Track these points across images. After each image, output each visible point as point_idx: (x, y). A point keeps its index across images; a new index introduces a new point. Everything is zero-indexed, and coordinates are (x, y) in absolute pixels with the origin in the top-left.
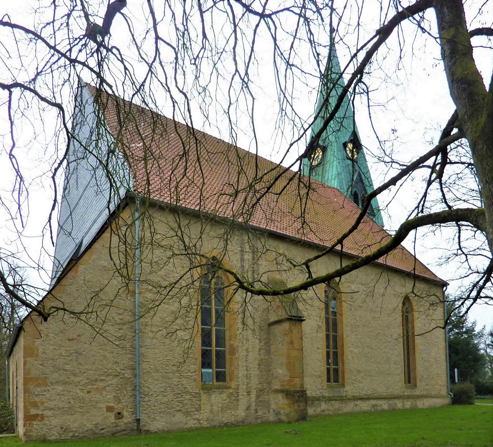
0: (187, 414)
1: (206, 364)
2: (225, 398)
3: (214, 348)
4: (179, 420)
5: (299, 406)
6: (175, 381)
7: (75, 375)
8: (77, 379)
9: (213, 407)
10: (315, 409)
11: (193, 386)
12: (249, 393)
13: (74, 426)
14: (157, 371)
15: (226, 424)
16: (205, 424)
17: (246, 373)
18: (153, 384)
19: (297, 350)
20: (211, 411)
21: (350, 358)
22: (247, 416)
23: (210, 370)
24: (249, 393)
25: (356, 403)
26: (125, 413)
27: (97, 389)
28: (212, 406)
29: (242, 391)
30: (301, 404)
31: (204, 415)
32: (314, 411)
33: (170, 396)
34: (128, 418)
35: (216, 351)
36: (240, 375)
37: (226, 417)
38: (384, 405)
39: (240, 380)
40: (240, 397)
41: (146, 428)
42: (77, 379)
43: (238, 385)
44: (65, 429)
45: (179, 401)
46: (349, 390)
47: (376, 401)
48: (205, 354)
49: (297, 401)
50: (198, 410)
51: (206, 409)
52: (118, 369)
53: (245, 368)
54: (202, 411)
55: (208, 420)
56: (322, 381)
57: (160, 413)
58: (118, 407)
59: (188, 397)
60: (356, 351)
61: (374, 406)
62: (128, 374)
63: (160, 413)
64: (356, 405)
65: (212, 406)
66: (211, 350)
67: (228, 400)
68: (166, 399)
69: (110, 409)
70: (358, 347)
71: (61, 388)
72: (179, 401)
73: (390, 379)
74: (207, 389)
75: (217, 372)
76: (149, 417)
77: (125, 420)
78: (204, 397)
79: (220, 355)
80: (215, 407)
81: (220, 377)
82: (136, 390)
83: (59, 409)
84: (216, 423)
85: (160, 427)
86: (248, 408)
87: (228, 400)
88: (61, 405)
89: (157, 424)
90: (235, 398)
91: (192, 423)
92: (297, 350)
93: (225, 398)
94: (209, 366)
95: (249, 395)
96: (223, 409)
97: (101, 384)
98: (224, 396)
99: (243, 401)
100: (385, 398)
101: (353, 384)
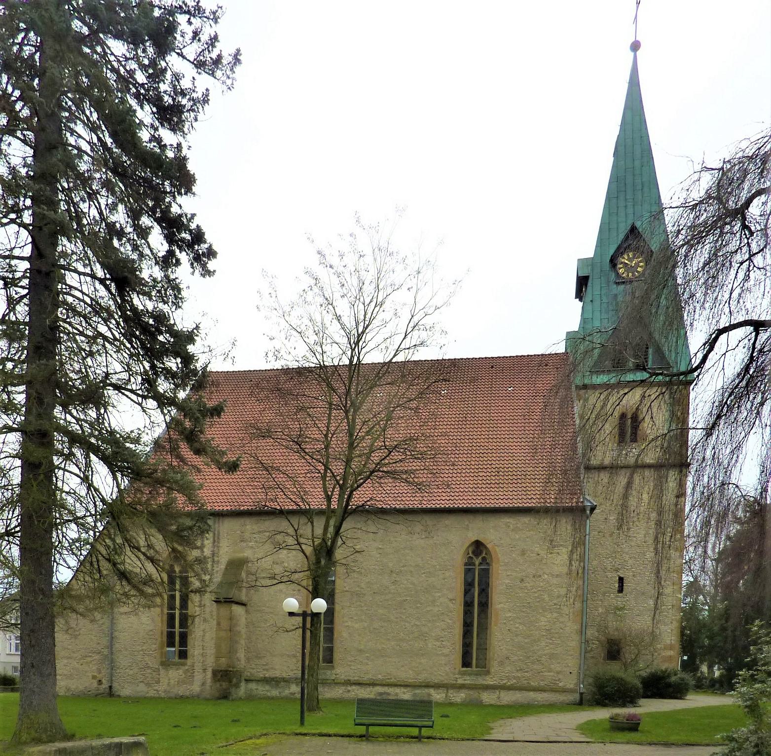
0: (148, 685)
1: (171, 644)
2: (181, 673)
3: (177, 630)
4: (142, 689)
5: (221, 685)
6: (139, 658)
7: (74, 652)
8: (75, 655)
9: (171, 680)
10: (281, 690)
11: (154, 663)
12: (205, 670)
13: (73, 687)
14: (126, 650)
15: (182, 697)
16: (163, 695)
17: (201, 651)
18: (122, 661)
19: (225, 630)
20: (169, 684)
21: (345, 635)
22: (202, 691)
23: (174, 649)
24: (205, 670)
25: (349, 688)
26: (104, 681)
27: (87, 662)
28: (169, 680)
29: (198, 667)
30: (224, 683)
31: (162, 687)
32: (280, 693)
33: (136, 670)
34: (105, 685)
35: (180, 632)
36: (195, 653)
37: (181, 691)
38: (405, 695)
39: (195, 658)
40: (196, 673)
41: (117, 694)
42: (75, 655)
43: (194, 663)
44: (68, 690)
45: (142, 674)
46: (498, 674)
47: (386, 688)
48: (171, 636)
49: (219, 681)
50: (158, 682)
51: (164, 681)
52: (100, 648)
53: (201, 647)
54: (161, 684)
55: (165, 691)
56: (298, 662)
57: (128, 682)
58: (99, 676)
59: (149, 671)
60: (356, 626)
61: (381, 694)
62: (106, 652)
63: (128, 682)
64: (349, 691)
65: (169, 680)
66: (175, 632)
67: (184, 676)
68: (131, 672)
69: (94, 677)
70: (362, 621)
71: (66, 661)
72: (142, 674)
73: (423, 661)
74: (166, 664)
75: (180, 651)
76: (120, 685)
77: (103, 686)
78: (162, 672)
79: (184, 638)
80: (172, 682)
81: (183, 655)
82: (112, 666)
83: (65, 675)
84: (172, 695)
85: (128, 694)
86: (203, 684)
87: (184, 676)
88: (66, 672)
89: (126, 691)
90: (190, 676)
91: (152, 693)
92: (225, 630)
93: (181, 673)
94: (174, 646)
95: (205, 672)
96: (180, 683)
97: (89, 659)
98: (181, 672)
99: (198, 677)
100: (406, 686)
101: (350, 666)
